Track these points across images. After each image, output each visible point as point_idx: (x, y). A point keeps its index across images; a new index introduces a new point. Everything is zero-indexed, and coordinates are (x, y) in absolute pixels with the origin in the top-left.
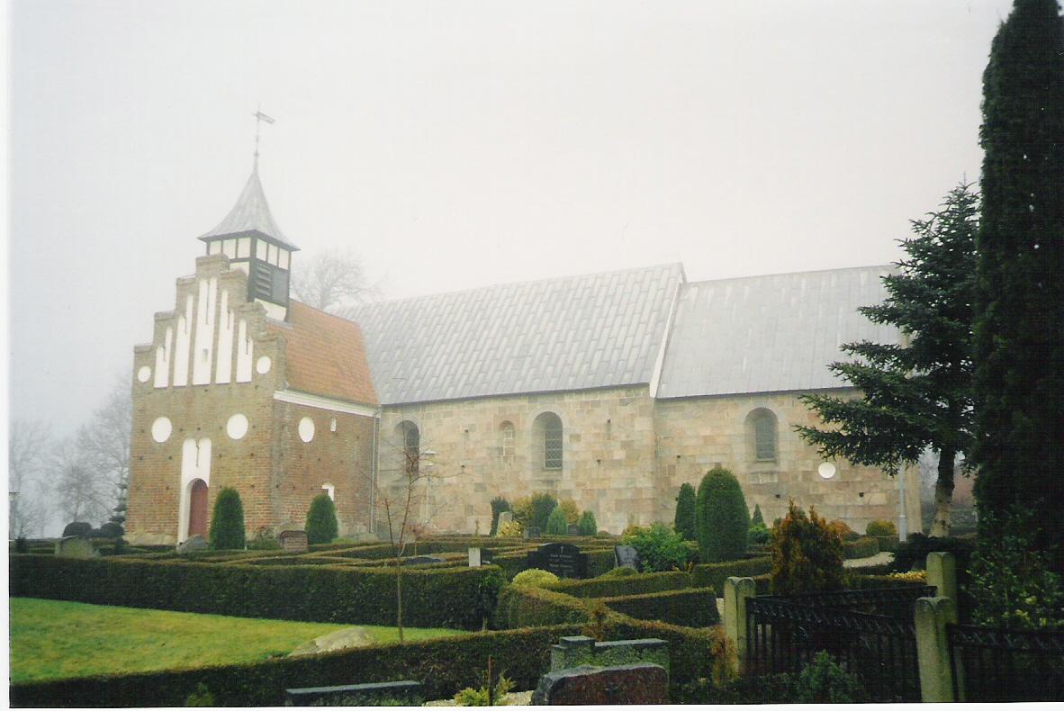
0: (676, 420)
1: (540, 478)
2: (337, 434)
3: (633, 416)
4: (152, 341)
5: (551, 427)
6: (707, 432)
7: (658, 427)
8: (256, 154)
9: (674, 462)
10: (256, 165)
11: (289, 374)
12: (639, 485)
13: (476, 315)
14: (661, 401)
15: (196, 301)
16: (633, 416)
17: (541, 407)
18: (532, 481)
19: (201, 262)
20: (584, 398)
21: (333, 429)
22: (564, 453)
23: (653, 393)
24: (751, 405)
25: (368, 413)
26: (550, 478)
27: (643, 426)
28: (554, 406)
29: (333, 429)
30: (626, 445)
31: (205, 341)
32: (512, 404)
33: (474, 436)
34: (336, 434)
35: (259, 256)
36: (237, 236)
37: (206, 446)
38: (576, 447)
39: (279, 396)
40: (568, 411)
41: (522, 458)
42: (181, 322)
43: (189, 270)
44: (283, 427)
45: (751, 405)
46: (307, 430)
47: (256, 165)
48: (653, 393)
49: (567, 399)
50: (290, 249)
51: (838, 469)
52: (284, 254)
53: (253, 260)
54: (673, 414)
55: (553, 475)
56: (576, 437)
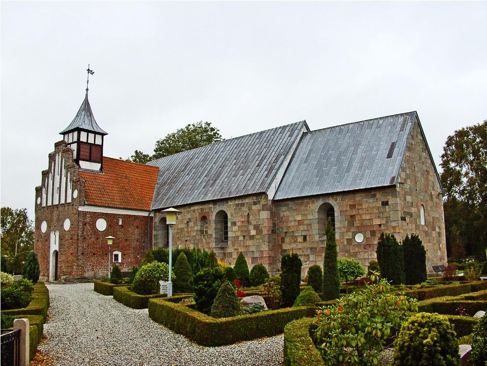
0: (284, 212)
1: (219, 246)
2: (123, 226)
3: (259, 211)
4: (41, 185)
5: (223, 217)
6: (299, 218)
7: (273, 215)
8: (87, 90)
9: (284, 235)
10: (87, 95)
11: (86, 197)
12: (262, 249)
13: (291, 146)
14: (274, 201)
15: (55, 164)
16: (259, 211)
17: (218, 208)
18: (215, 248)
19: (57, 145)
20: (237, 202)
21: (120, 223)
22: (336, 234)
23: (270, 197)
24: (320, 202)
25: (146, 214)
26: (223, 246)
27: (265, 215)
28: (224, 207)
29: (120, 223)
30: (256, 227)
31: (57, 185)
32: (205, 207)
33: (191, 224)
34: (122, 226)
35: (82, 140)
36: (72, 131)
37: (57, 234)
38: (235, 228)
39: (81, 209)
40: (229, 209)
41: (211, 235)
42: (50, 175)
43: (52, 149)
44: (85, 224)
45: (320, 202)
46: (101, 225)
47: (87, 95)
48: (270, 197)
49: (230, 203)
50: (103, 135)
51: (365, 237)
52: (99, 137)
53: (79, 142)
54: (284, 209)
55: (223, 244)
56: (234, 224)
